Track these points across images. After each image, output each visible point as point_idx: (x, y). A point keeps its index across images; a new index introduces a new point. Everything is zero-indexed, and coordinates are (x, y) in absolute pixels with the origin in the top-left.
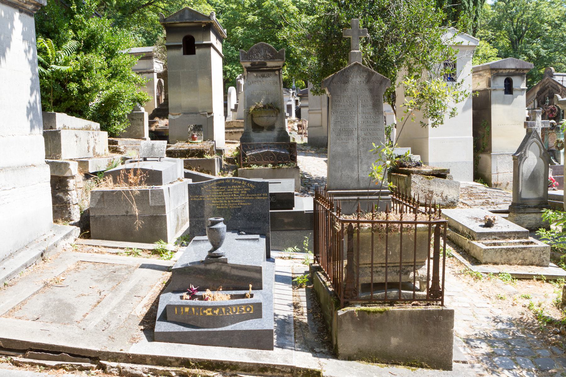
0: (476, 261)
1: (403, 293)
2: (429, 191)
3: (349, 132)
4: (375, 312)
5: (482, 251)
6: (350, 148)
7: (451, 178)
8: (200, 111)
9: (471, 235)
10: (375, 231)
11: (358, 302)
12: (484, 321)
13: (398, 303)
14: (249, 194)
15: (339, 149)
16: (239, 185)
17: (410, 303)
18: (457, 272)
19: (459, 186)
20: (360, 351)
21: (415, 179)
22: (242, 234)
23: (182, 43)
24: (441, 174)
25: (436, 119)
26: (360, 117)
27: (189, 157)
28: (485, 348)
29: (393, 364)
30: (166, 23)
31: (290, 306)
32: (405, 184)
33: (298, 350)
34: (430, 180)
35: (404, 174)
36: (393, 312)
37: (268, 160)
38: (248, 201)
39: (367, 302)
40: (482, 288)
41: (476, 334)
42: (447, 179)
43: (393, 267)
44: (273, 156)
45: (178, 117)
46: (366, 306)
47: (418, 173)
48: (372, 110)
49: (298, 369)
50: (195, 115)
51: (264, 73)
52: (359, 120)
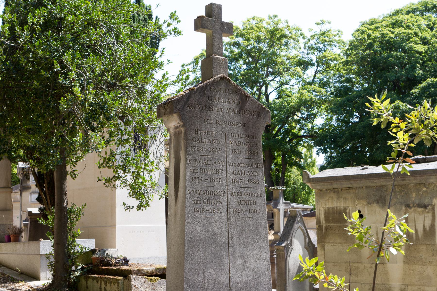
3: (213, 198)
6: (216, 228)
26: (230, 169)
48: (247, 161)
52: (229, 176)
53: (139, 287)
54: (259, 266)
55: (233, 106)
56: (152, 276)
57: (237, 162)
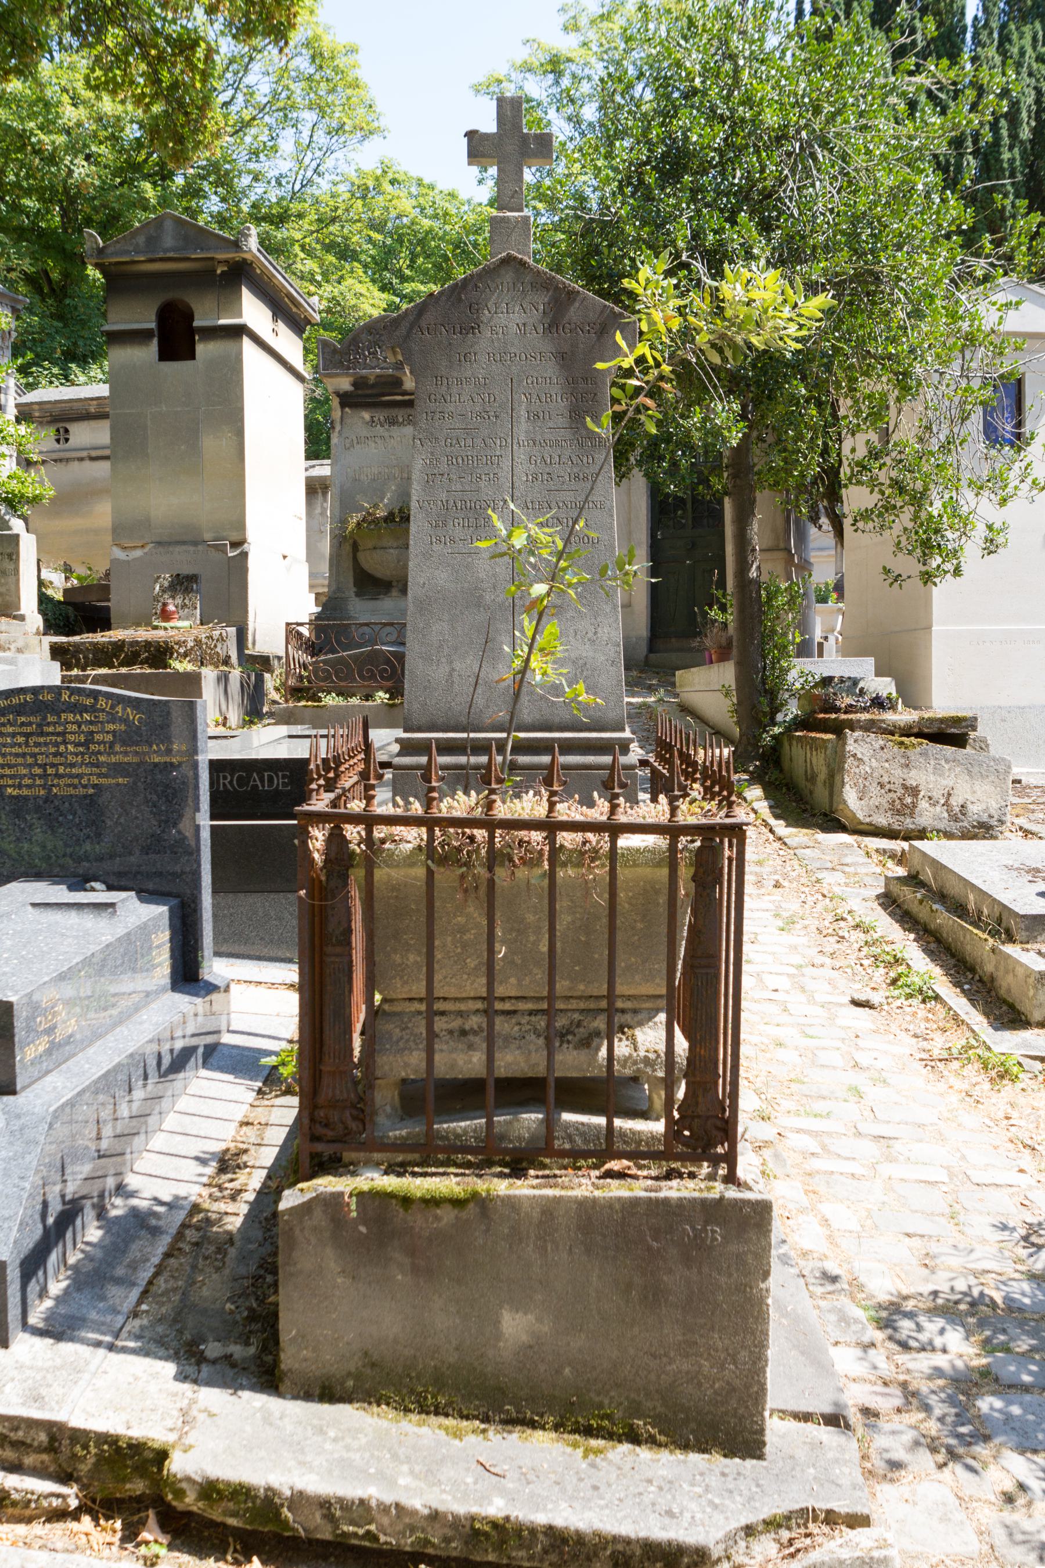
0: (1009, 1015)
1: (568, 1125)
2: (905, 787)
4: (432, 1202)
5: (1031, 980)
6: (482, 575)
7: (983, 746)
8: (207, 536)
9: (1005, 925)
10: (443, 860)
11: (377, 1156)
12: (984, 1241)
13: (544, 1167)
14: (124, 743)
15: (443, 577)
16: (85, 709)
17: (596, 1167)
18: (936, 1053)
19: (1007, 772)
20: (373, 1365)
21: (856, 744)
22: (93, 890)
23: (153, 325)
24: (951, 734)
25: (939, 560)
26: (521, 455)
27: (122, 664)
28: (959, 1348)
29: (511, 1422)
30: (107, 261)
31: (202, 1161)
32: (828, 766)
33: (124, 1350)
34: (909, 753)
35: (826, 732)
36: (511, 1202)
37: (372, 677)
38: (118, 769)
39: (416, 1157)
40: (1015, 1114)
41: (935, 1294)
42: (969, 750)
43: (531, 1013)
44: (338, 642)
45: (138, 553)
46: (400, 1175)
47: (870, 727)
48: (567, 434)
49: (79, 1437)
50: (192, 548)
51: (394, 412)
52: (519, 469)
53: (866, 759)
54: (591, 654)
55: (535, 316)
56: (908, 736)
57: (538, 438)
